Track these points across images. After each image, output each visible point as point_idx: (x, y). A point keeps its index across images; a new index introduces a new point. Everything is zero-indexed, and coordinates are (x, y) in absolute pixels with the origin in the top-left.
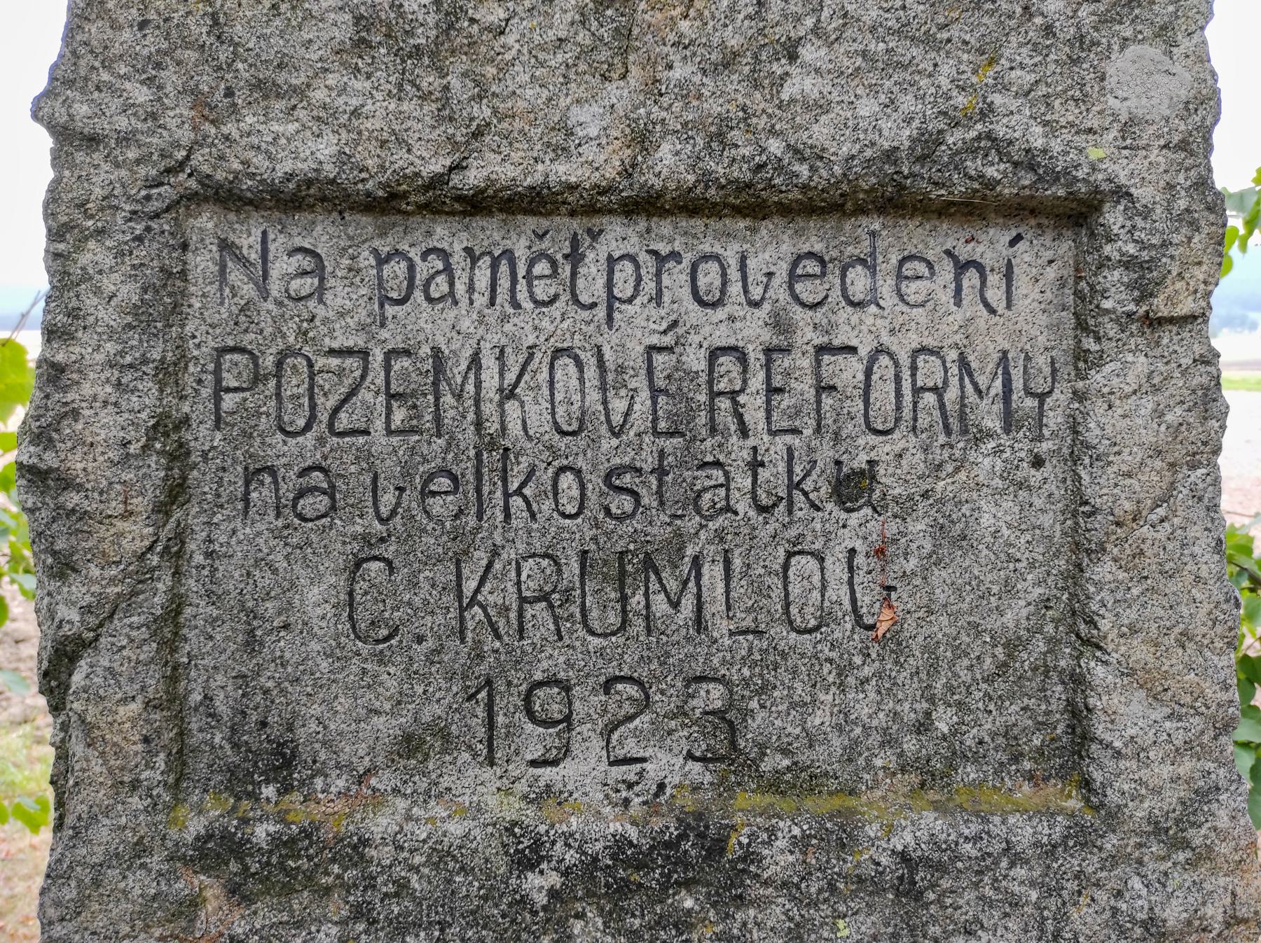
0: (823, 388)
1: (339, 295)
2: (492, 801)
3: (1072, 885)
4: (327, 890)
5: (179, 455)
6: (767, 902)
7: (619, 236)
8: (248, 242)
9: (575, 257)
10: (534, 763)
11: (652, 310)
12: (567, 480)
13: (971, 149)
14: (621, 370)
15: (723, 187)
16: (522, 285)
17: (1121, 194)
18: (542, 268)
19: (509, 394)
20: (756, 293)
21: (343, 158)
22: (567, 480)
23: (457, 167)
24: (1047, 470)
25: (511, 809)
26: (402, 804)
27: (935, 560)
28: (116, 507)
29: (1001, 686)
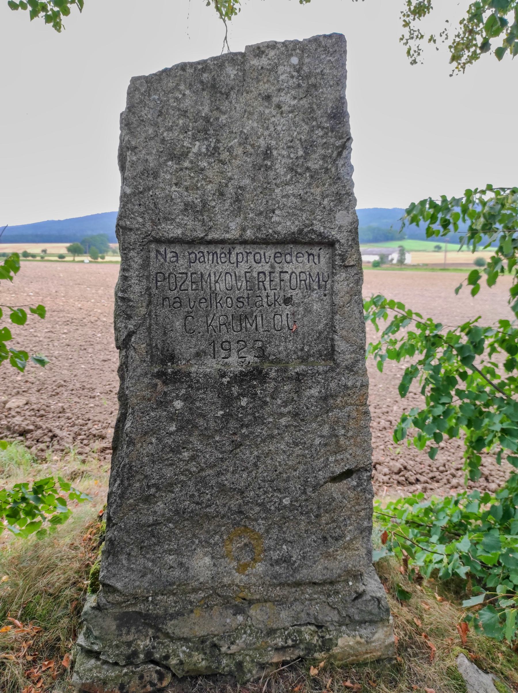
0: (281, 280)
1: (181, 262)
2: (215, 366)
3: (330, 379)
4: (183, 382)
5: (150, 295)
6: (270, 383)
7: (239, 249)
8: (162, 250)
9: (230, 253)
10: (223, 358)
11: (246, 264)
12: (229, 300)
13: (309, 232)
14: (240, 277)
15: (265, 119)
16: (219, 259)
17: (338, 241)
18: (223, 255)
19: (216, 282)
20: (267, 260)
21: (183, 234)
22: (229, 300)
23: (206, 235)
24: (327, 297)
25: (219, 367)
26: (196, 366)
27: (304, 316)
28: (140, 305)
29: (318, 341)
